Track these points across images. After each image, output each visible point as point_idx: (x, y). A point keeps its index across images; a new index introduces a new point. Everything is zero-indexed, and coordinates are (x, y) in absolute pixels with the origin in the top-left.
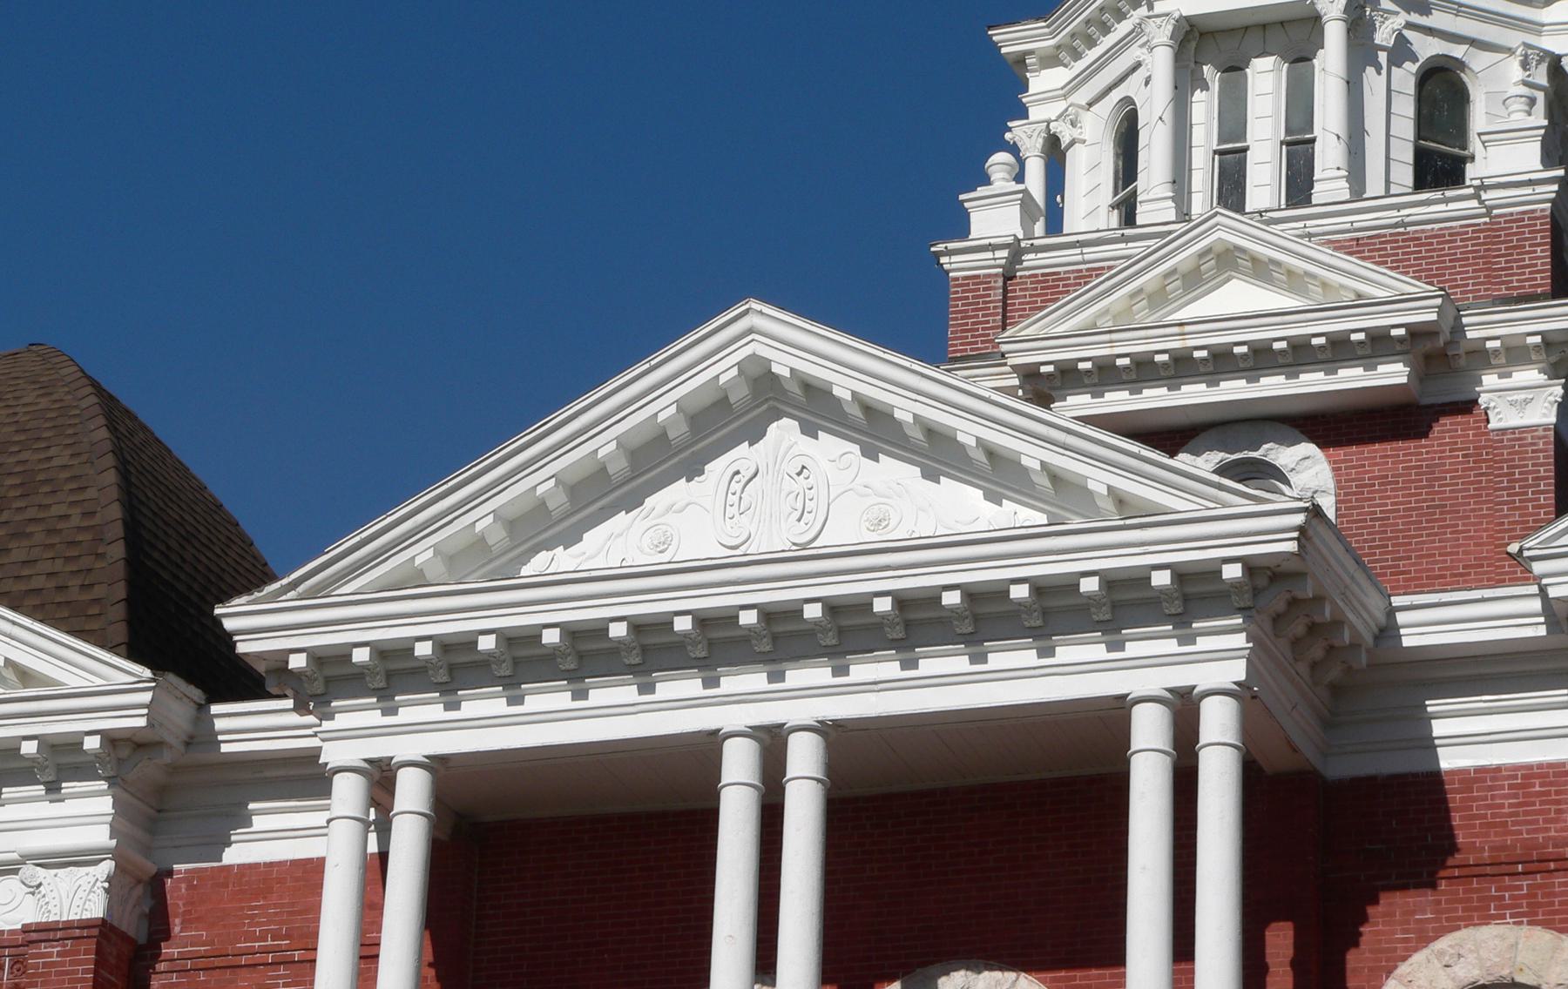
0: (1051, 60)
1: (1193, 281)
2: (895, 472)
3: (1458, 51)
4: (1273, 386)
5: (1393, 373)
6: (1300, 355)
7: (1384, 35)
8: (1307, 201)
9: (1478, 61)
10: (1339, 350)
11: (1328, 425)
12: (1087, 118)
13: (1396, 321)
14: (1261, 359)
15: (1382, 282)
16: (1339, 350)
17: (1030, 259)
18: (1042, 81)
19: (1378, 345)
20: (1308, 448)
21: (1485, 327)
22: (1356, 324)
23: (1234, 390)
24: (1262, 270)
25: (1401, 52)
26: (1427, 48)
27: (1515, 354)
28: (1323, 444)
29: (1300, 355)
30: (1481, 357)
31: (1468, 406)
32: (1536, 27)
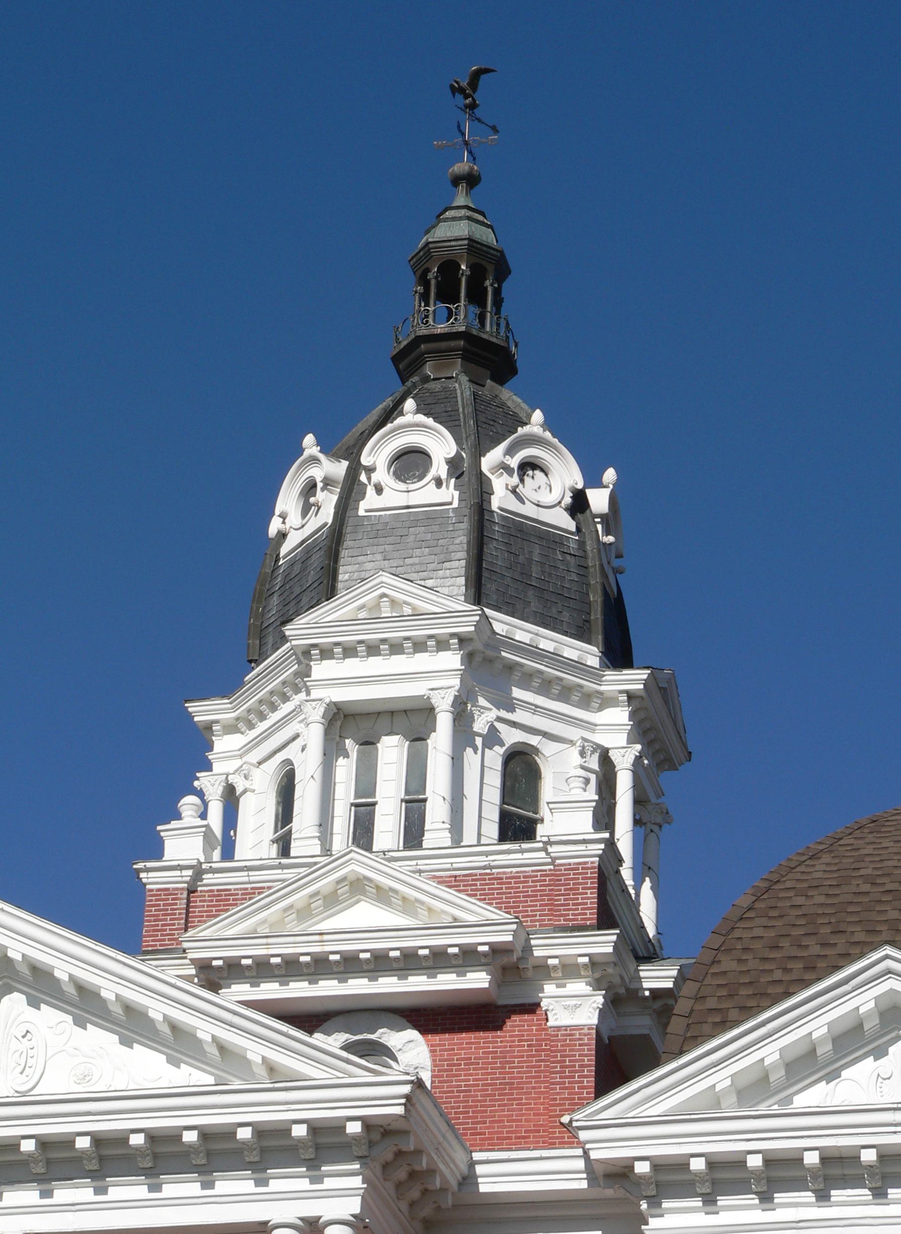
0: (232, 728)
1: (332, 901)
2: (99, 1038)
3: (534, 740)
4: (388, 985)
5: (478, 980)
6: (410, 962)
7: (480, 725)
8: (419, 845)
9: (548, 748)
10: (439, 960)
11: (429, 1017)
12: (257, 773)
13: (482, 940)
14: (380, 964)
15: (474, 910)
16: (439, 960)
17: (208, 878)
18: (223, 744)
19: (468, 958)
20: (412, 1034)
21: (548, 948)
22: (453, 941)
23: (358, 986)
24: (383, 896)
25: (492, 738)
26: (511, 737)
27: (569, 970)
28: (424, 1031)
29: (410, 962)
30: (544, 971)
31: (532, 1008)
32: (591, 726)
